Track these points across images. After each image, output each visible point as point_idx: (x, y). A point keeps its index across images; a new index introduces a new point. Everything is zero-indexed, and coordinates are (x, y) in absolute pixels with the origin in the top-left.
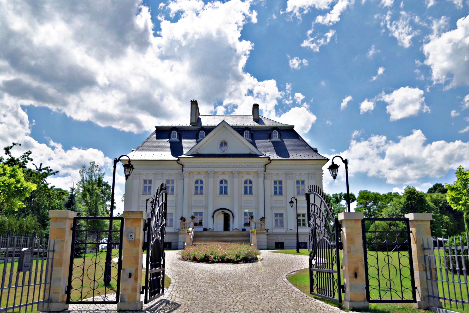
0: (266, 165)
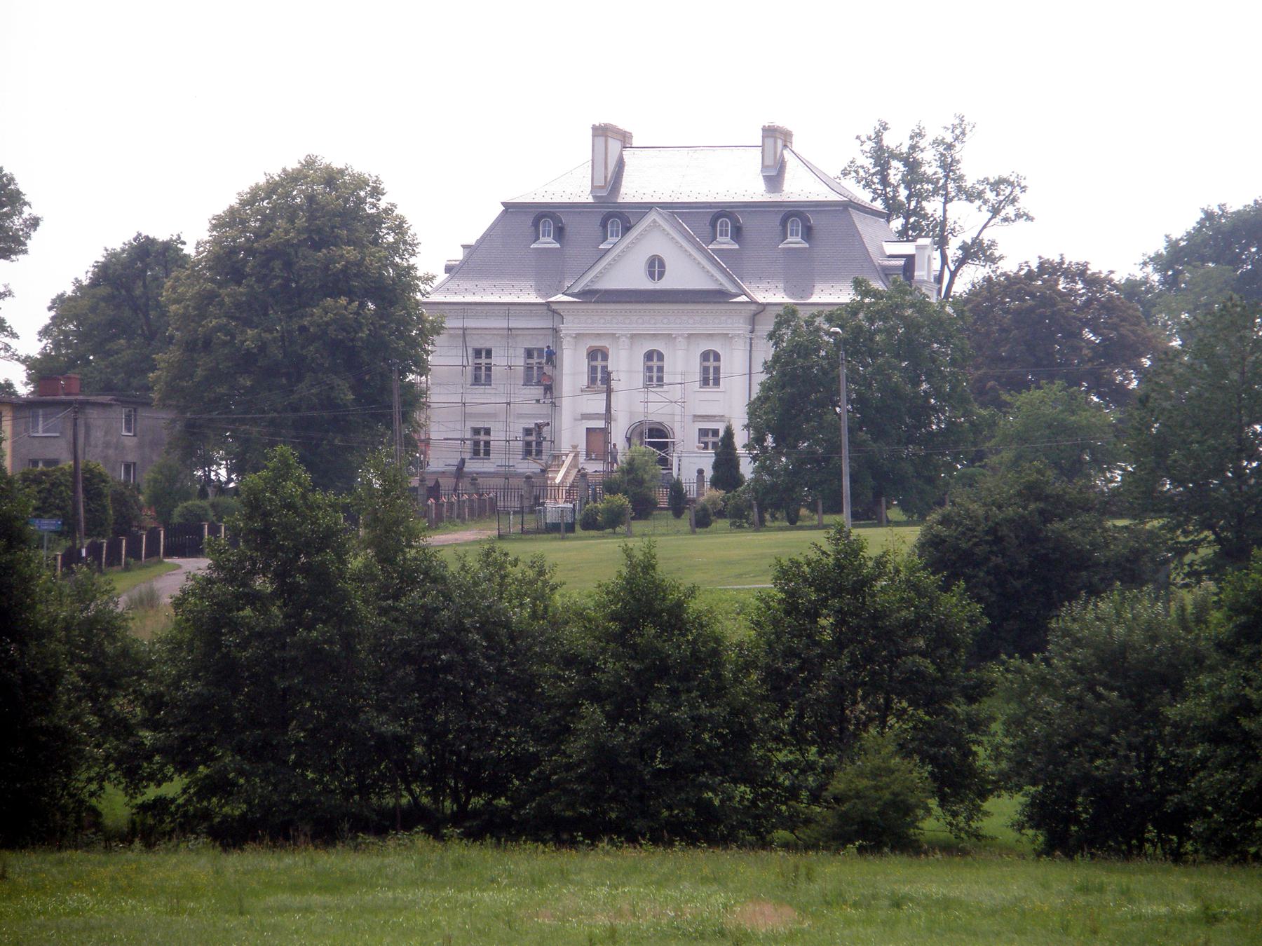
0: (755, 315)
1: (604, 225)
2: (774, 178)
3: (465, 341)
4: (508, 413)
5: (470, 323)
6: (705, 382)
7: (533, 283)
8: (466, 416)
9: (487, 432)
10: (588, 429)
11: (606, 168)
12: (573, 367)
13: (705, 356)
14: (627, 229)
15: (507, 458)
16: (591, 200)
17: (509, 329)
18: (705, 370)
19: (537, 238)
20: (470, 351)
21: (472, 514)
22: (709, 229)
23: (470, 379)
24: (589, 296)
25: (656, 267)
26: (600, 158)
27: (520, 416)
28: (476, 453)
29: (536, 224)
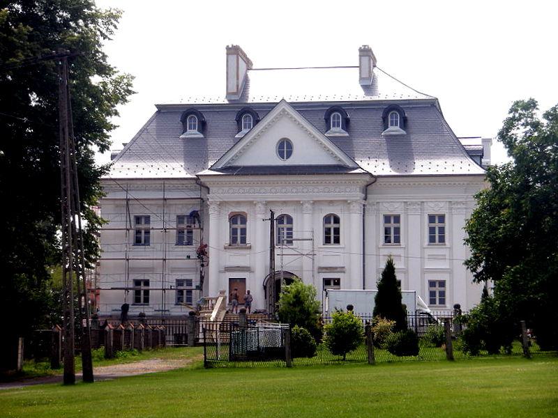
0: (367, 186)
1: (239, 121)
2: (369, 87)
3: (128, 210)
4: (164, 266)
5: (132, 195)
6: (327, 240)
7: (183, 164)
8: (129, 270)
9: (147, 283)
10: (230, 279)
11: (238, 79)
12: (217, 230)
13: (327, 219)
14: (257, 122)
15: (162, 302)
16: (226, 102)
17: (165, 199)
18: (327, 231)
19: (185, 131)
20: (132, 218)
21: (147, 344)
22: (323, 122)
23: (132, 241)
24: (230, 170)
25: (285, 147)
26: (233, 72)
27: (173, 270)
28: (137, 300)
29: (184, 121)
